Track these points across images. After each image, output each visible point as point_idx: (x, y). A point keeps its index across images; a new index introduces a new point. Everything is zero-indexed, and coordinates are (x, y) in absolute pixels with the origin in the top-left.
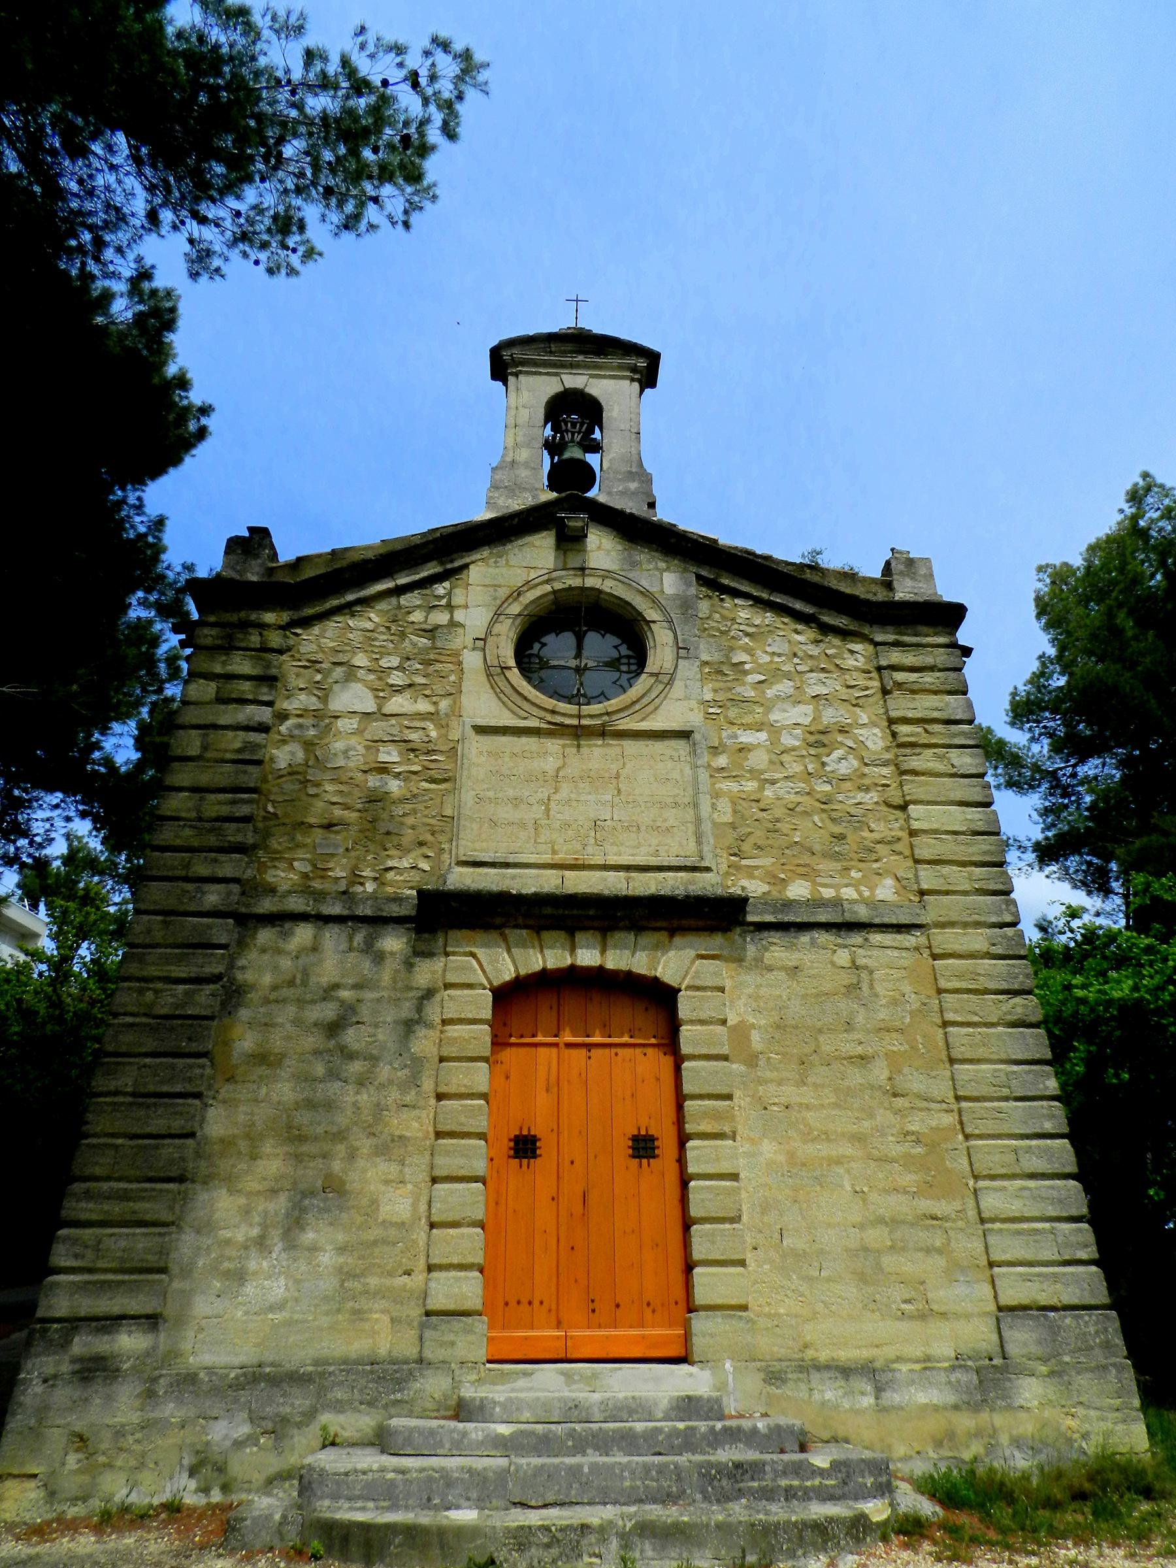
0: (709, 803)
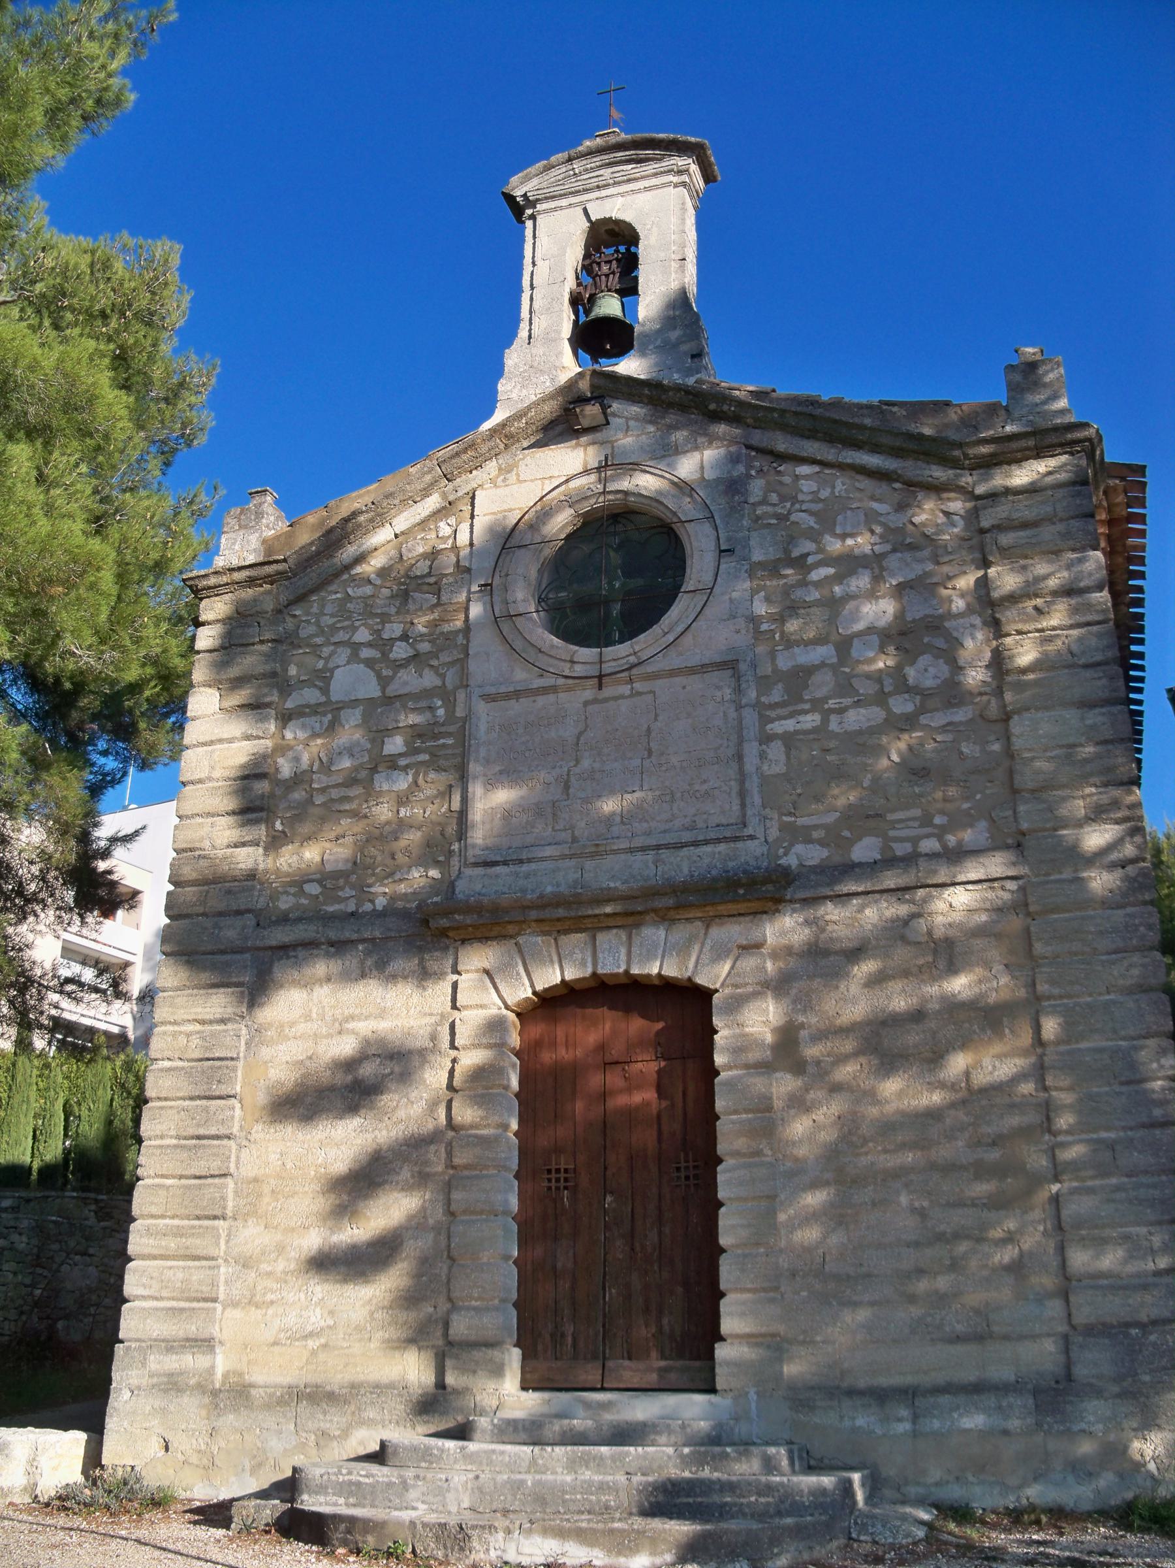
0: (755, 752)
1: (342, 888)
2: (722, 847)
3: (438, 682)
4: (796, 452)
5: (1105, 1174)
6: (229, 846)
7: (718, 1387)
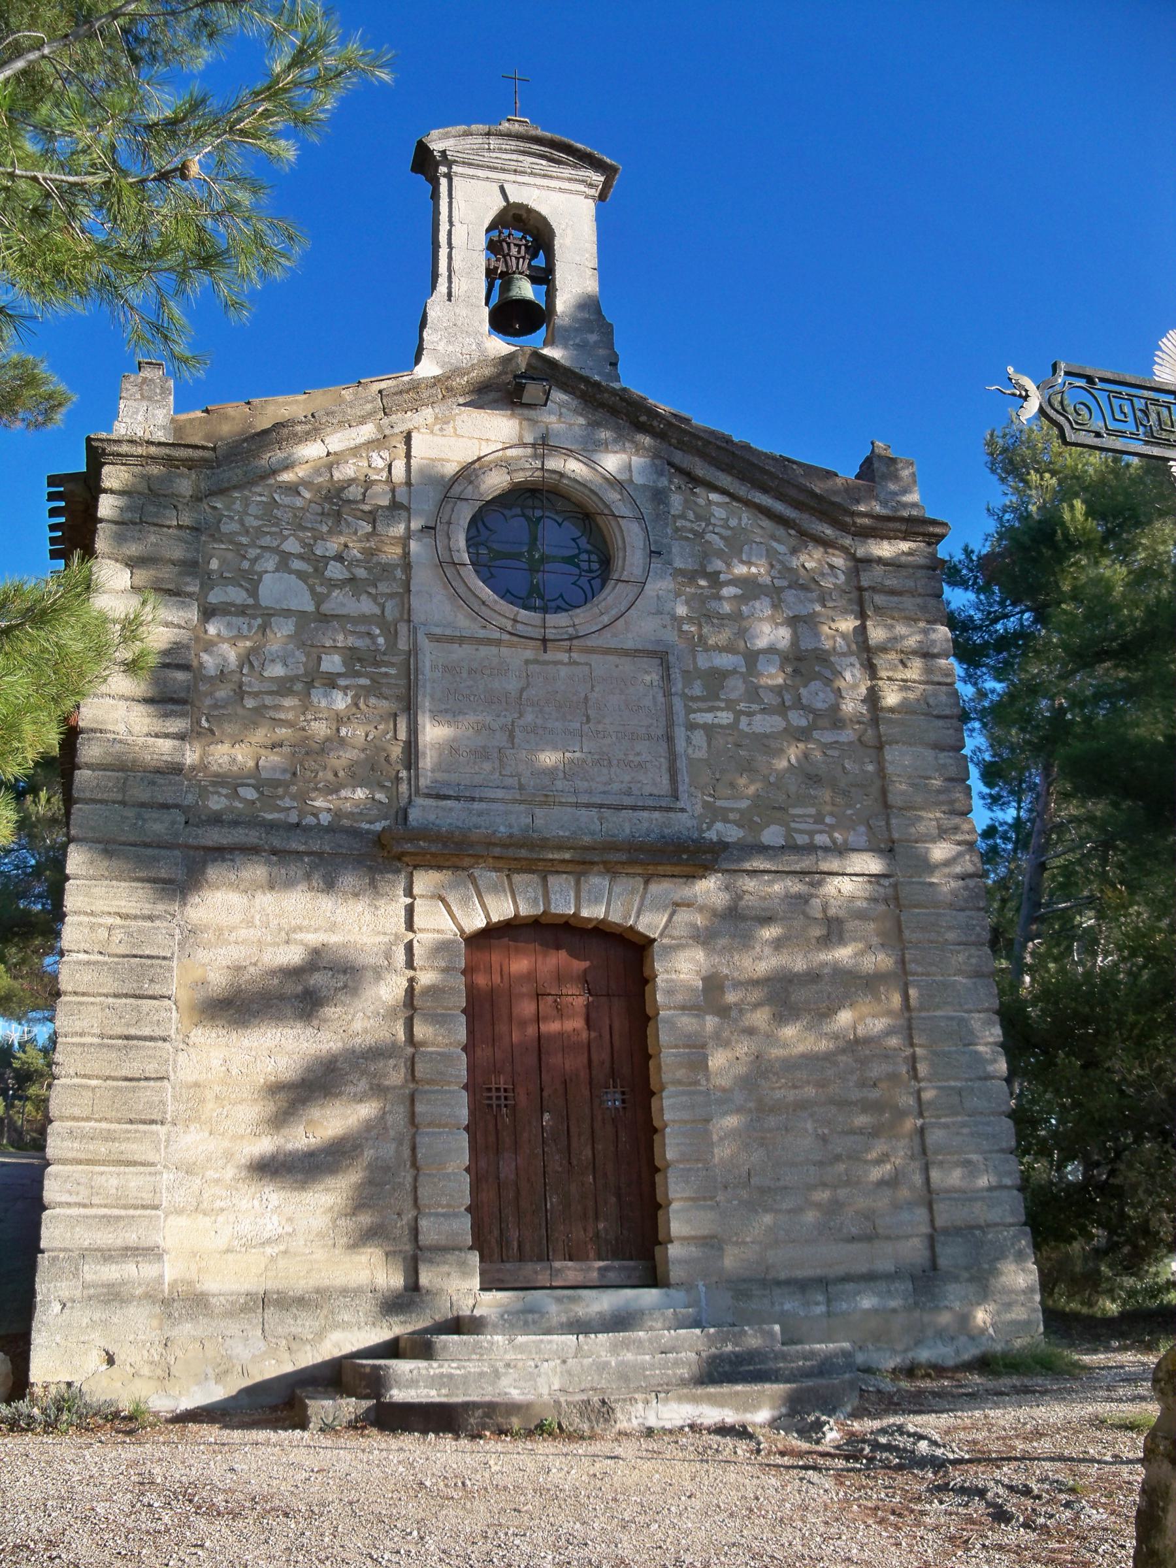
1: (281, 798)
2: (656, 815)
3: (378, 611)
4: (712, 480)
5: (956, 1114)
6: (148, 735)
7: (672, 1281)
